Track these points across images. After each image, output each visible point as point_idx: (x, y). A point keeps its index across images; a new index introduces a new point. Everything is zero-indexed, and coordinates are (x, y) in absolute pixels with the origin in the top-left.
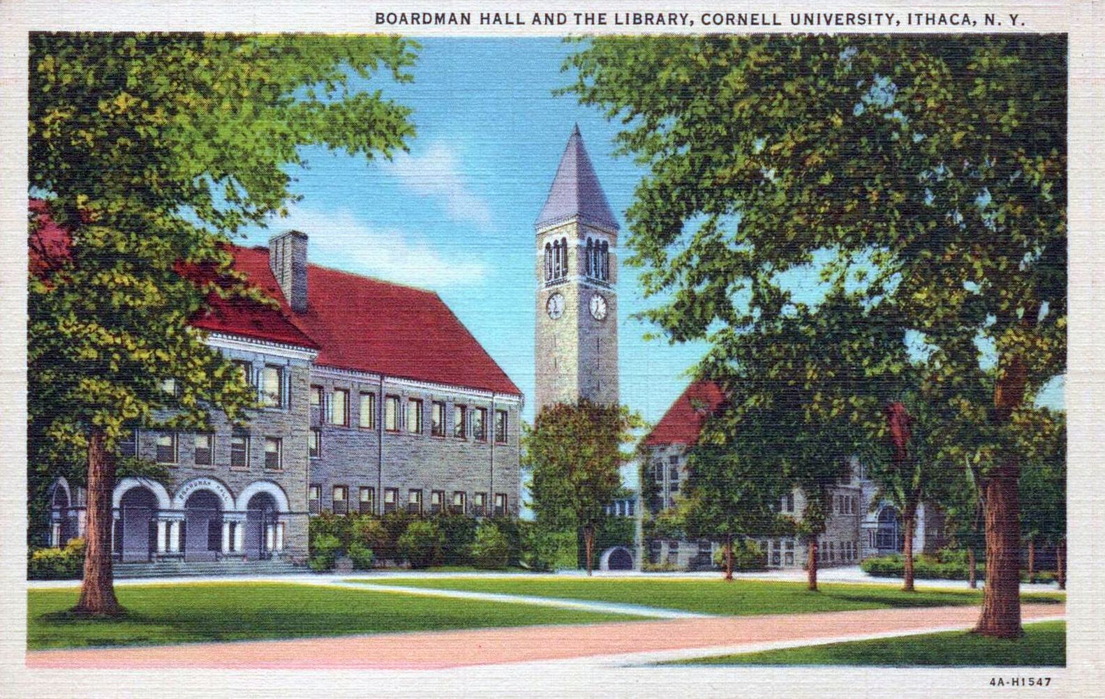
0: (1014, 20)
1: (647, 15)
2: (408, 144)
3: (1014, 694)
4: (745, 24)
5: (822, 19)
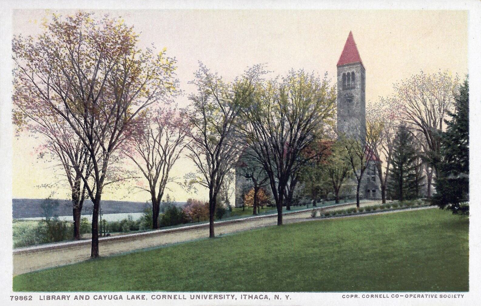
0: (287, 297)
1: (52, 296)
2: (420, 74)
3: (267, 304)
4: (171, 298)
5: (203, 297)
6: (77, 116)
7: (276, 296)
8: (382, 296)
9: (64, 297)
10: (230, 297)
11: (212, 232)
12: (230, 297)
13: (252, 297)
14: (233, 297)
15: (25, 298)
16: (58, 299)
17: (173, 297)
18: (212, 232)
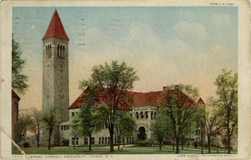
6: (174, 117)
7: (106, 156)
8: (58, 157)
9: (39, 157)
10: (84, 157)
11: (90, 148)
12: (84, 157)
13: (95, 157)
14: (85, 156)
15: (213, 4)
16: (51, 157)
17: (56, 157)
18: (90, 148)
